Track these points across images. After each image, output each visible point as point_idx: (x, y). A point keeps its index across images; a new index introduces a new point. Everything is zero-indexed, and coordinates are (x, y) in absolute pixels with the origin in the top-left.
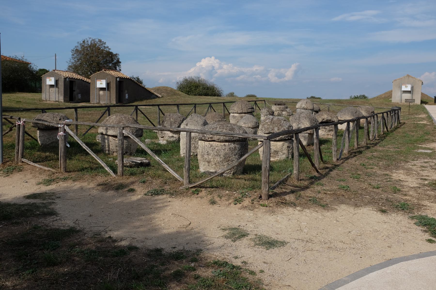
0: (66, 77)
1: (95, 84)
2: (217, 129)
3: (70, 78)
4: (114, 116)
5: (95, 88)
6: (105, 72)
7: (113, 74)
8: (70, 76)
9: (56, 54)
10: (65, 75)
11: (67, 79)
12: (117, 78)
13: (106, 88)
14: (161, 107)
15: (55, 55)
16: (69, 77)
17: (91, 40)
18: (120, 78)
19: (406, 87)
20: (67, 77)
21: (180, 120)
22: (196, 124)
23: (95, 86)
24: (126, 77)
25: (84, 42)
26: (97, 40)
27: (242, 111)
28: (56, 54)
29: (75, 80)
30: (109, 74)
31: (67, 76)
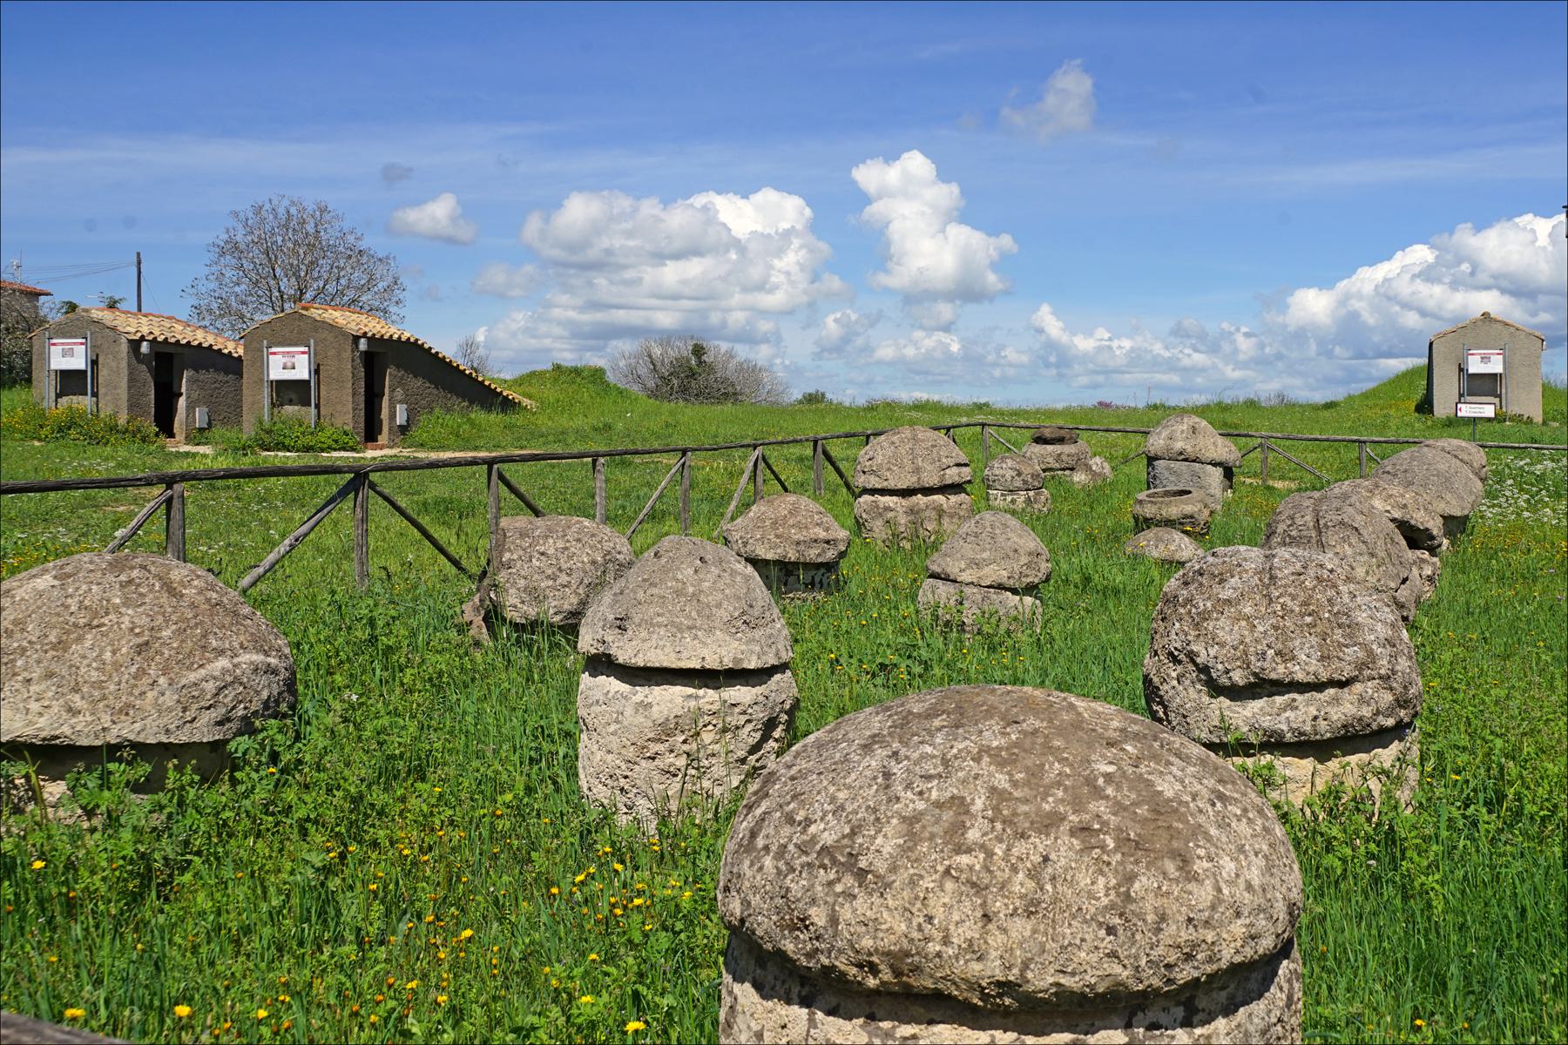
0: (139, 335)
1: (261, 365)
2: (959, 828)
3: (154, 342)
4: (45, 582)
5: (262, 380)
6: (304, 312)
7: (341, 321)
8: (157, 333)
9: (139, 254)
10: (133, 330)
11: (145, 348)
12: (356, 339)
13: (86, 371)
14: (508, 469)
15: (135, 259)
16: (151, 338)
17: (286, 203)
18: (372, 340)
19: (1485, 359)
20: (143, 338)
21: (594, 562)
22: (689, 617)
23: (262, 373)
24: (395, 337)
25: (258, 210)
26: (311, 207)
27: (915, 479)
28: (139, 254)
29: (180, 350)
30: (324, 322)
31: (145, 330)
